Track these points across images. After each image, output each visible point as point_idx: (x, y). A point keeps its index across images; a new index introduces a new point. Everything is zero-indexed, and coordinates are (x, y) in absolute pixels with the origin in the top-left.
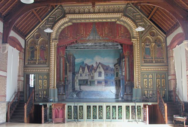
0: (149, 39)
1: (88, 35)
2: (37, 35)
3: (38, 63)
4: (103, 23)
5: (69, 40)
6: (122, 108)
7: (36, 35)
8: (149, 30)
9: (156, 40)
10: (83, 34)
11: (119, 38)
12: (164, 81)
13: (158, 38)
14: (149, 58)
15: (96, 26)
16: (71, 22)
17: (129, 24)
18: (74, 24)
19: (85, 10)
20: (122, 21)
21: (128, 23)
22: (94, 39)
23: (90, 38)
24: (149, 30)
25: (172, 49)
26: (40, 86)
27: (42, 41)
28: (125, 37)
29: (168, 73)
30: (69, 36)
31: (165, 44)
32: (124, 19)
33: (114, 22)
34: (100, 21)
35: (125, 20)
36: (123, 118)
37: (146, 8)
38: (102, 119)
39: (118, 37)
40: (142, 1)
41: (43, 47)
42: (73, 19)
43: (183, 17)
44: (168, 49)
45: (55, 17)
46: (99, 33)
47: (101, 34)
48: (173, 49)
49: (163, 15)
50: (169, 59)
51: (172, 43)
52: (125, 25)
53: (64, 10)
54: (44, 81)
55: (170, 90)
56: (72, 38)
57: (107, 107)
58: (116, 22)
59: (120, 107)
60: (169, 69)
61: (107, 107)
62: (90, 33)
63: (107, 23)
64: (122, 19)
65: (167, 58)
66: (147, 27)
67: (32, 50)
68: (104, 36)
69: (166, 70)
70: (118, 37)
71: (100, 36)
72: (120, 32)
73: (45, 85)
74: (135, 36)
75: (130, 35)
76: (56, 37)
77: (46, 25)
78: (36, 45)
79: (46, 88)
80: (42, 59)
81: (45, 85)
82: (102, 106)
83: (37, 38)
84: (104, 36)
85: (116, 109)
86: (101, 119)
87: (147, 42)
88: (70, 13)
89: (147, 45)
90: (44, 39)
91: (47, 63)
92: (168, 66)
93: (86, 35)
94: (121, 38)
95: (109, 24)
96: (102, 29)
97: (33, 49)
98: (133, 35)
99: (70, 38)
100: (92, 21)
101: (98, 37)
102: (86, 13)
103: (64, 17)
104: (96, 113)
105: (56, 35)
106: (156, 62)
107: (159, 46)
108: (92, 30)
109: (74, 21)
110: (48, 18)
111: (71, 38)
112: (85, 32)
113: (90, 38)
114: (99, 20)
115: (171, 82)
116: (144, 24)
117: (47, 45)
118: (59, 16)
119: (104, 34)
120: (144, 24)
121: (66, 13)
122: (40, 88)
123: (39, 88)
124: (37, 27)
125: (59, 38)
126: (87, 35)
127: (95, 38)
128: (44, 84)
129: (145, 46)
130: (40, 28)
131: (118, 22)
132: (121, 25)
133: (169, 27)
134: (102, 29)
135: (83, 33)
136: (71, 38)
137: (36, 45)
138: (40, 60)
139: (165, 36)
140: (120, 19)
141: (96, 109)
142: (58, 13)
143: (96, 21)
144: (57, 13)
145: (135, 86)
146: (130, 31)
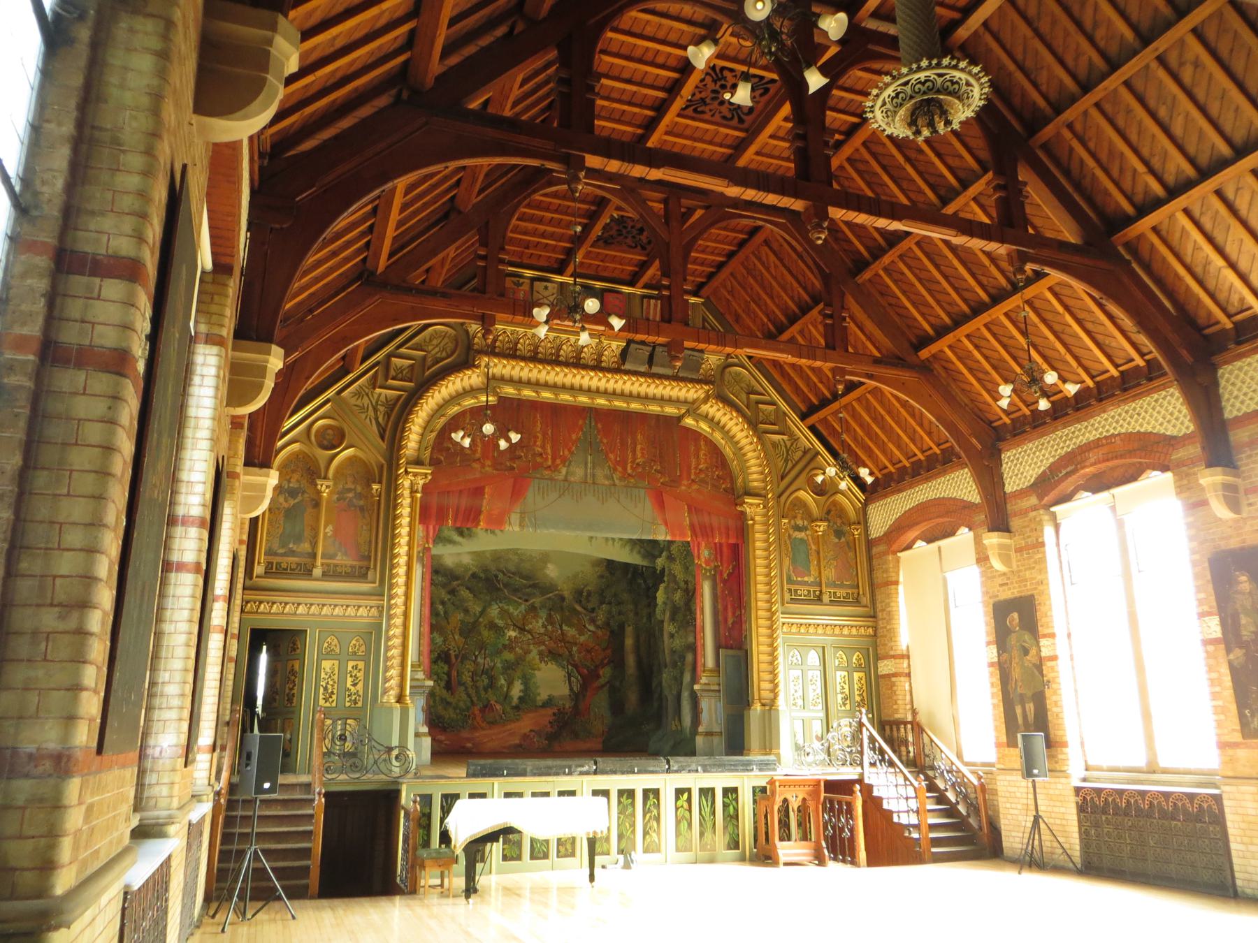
0: (802, 504)
1: (564, 460)
2: (326, 428)
3: (324, 574)
5: (478, 475)
6: (736, 800)
8: (806, 466)
9: (828, 512)
11: (689, 486)
12: (863, 681)
13: (835, 503)
14: (805, 583)
15: (600, 426)
16: (495, 394)
17: (732, 433)
18: (503, 400)
20: (706, 418)
21: (727, 428)
22: (589, 480)
24: (806, 466)
25: (895, 553)
26: (326, 689)
27: (351, 460)
28: (713, 485)
29: (875, 649)
30: (478, 455)
31: (861, 527)
32: (712, 411)
33: (671, 417)
34: (619, 404)
35: (718, 415)
37: (807, 379)
38: (659, 851)
39: (685, 482)
40: (849, 368)
41: (351, 495)
42: (502, 379)
43: (979, 447)
44: (875, 550)
45: (424, 358)
46: (612, 456)
47: (618, 463)
50: (877, 592)
51: (899, 528)
52: (717, 437)
53: (467, 332)
54: (351, 664)
55: (884, 718)
56: (494, 466)
57: (679, 792)
58: (679, 418)
59: (652, 794)
61: (679, 792)
62: (572, 453)
63: (643, 417)
64: (705, 408)
66: (799, 454)
67: (292, 502)
68: (629, 471)
69: (870, 636)
70: (685, 482)
71: (615, 470)
74: (756, 488)
75: (732, 479)
77: (378, 390)
78: (319, 482)
79: (360, 704)
80: (345, 554)
81: (354, 685)
82: (656, 792)
83: (325, 443)
84: (629, 471)
85: (713, 802)
87: (799, 516)
88: (492, 351)
89: (798, 529)
90: (360, 454)
91: (370, 574)
93: (554, 459)
94: (695, 487)
95: (653, 422)
96: (623, 444)
98: (745, 481)
99: (483, 466)
100: (583, 399)
101: (606, 471)
102: (566, 364)
103: (465, 363)
106: (326, 576)
107: (839, 534)
108: (579, 439)
109: (509, 391)
110: (389, 356)
111: (489, 462)
112: (552, 447)
114: (617, 403)
116: (789, 444)
117: (375, 487)
118: (443, 359)
119: (633, 462)
120: (789, 444)
121: (476, 347)
122: (326, 700)
123: (322, 702)
124: (330, 393)
126: (558, 461)
128: (349, 680)
130: (344, 400)
131: (689, 422)
132: (696, 435)
133: (886, 467)
134: (623, 444)
135: (543, 447)
136: (489, 462)
137: (319, 482)
139: (862, 497)
140: (698, 408)
141: (633, 804)
142: (435, 342)
143: (601, 401)
144: (431, 340)
145: (756, 697)
146: (735, 465)
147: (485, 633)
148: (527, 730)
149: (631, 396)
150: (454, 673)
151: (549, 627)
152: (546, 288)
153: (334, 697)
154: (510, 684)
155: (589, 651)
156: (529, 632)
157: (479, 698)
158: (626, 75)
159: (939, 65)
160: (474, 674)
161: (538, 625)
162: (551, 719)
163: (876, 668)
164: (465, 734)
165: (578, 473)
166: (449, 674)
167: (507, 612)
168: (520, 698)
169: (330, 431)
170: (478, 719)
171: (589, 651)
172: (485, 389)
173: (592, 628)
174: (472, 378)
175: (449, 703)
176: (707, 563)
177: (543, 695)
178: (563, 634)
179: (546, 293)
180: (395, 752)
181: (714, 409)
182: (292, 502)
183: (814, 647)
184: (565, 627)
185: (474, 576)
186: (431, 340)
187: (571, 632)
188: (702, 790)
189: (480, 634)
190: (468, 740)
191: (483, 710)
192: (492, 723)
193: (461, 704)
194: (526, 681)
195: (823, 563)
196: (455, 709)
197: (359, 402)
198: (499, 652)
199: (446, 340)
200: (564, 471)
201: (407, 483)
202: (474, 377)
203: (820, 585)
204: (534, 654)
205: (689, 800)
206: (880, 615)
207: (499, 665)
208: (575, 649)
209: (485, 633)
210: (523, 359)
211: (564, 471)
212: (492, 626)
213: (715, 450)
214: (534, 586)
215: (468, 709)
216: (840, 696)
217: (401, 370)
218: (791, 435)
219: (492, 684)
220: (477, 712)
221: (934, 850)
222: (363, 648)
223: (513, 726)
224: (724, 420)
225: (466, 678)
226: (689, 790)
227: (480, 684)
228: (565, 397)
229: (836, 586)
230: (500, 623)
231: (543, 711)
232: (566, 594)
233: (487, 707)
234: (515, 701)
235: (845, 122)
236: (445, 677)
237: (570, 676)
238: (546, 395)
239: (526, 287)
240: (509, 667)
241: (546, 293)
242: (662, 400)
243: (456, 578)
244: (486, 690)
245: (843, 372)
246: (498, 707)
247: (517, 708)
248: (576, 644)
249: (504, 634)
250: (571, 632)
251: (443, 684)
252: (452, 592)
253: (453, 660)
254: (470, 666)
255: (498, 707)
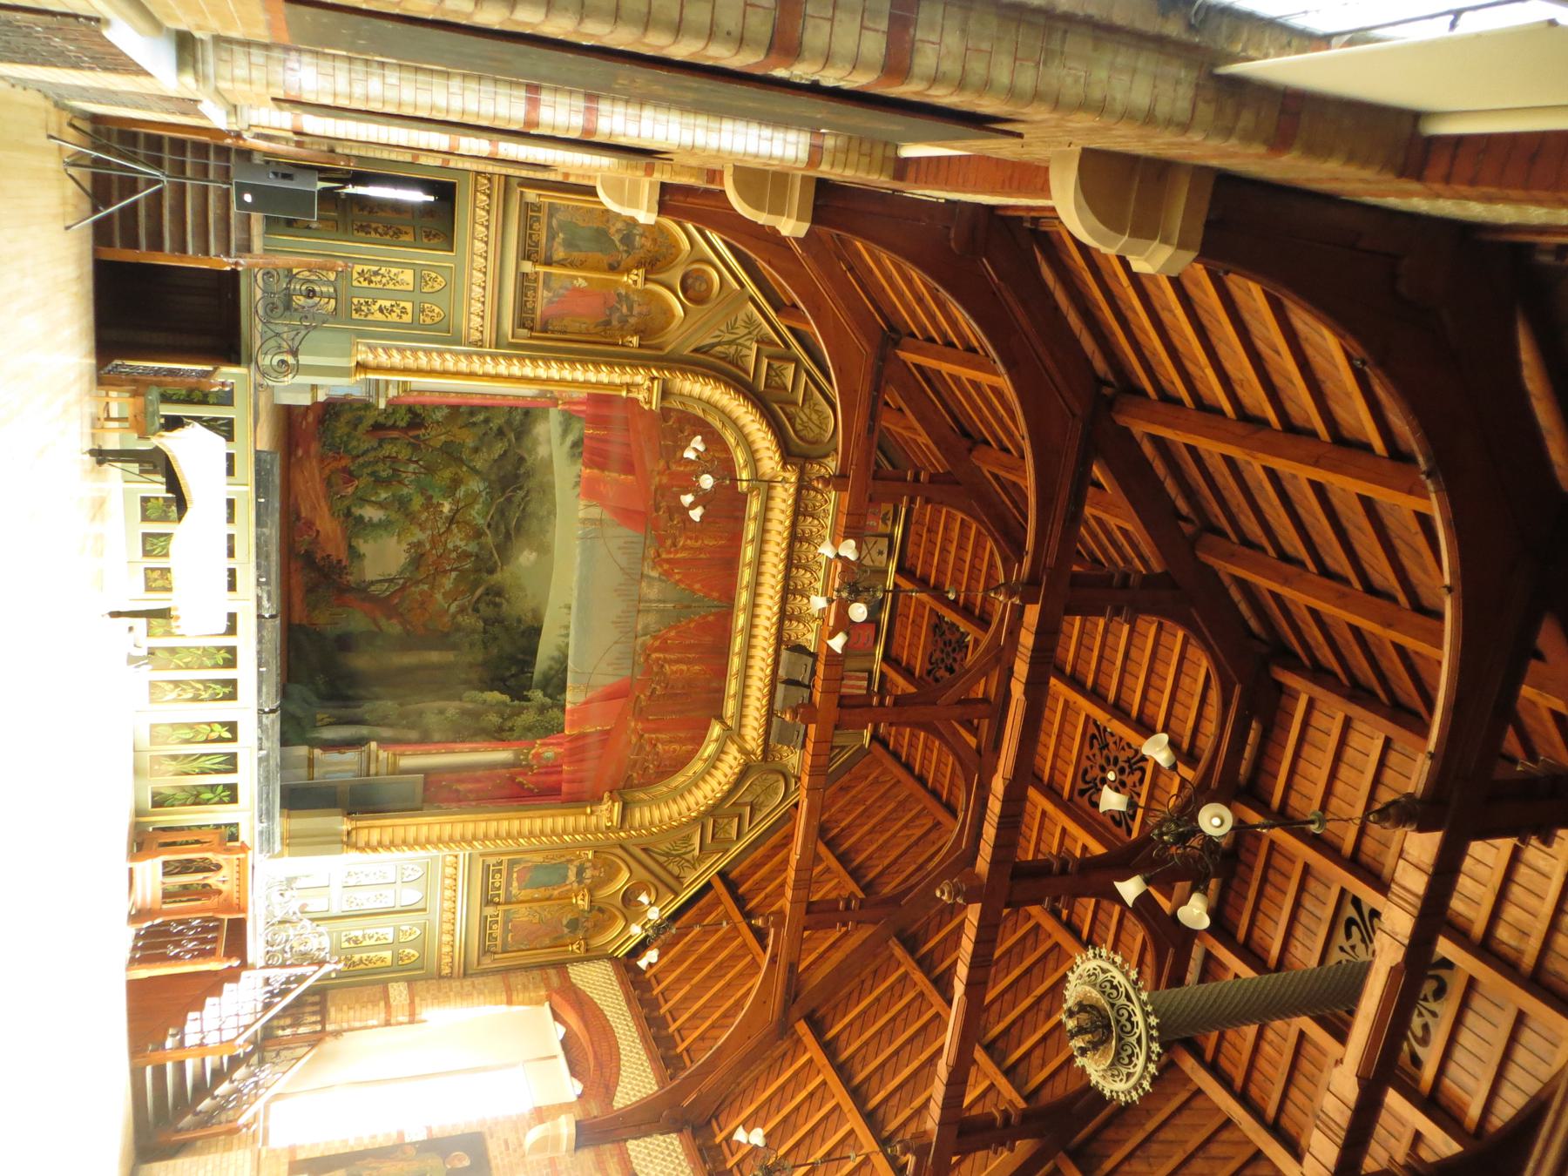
1: (668, 574)
3: (525, 275)
4: (721, 651)
6: (221, 802)
7: (704, 271)
9: (601, 910)
10: (674, 545)
12: (379, 964)
13: (613, 919)
14: (509, 884)
15: (711, 618)
16: (751, 490)
18: (742, 499)
19: (806, 568)
20: (721, 751)
23: (650, 586)
25: (549, 998)
26: (376, 273)
27: (668, 312)
28: (635, 762)
29: (426, 978)
30: (674, 467)
31: (581, 953)
34: (738, 643)
36: (156, 706)
39: (640, 726)
40: (784, 932)
41: (625, 310)
42: (769, 498)
43: (686, 1103)
44: (552, 972)
45: (795, 403)
46: (673, 633)
47: (665, 641)
48: (547, 1004)
49: (721, 968)
50: (498, 978)
52: (697, 766)
53: (826, 456)
54: (409, 306)
55: (331, 993)
56: (660, 487)
57: (232, 727)
58: (720, 718)
60: (445, 984)
61: (232, 727)
63: (722, 673)
64: (733, 750)
65: (506, 971)
66: (676, 871)
67: (616, 238)
68: (654, 656)
70: (640, 726)
71: (655, 638)
72: (662, 736)
73: (381, 310)
74: (632, 816)
75: (643, 786)
76: (681, 395)
77: (755, 346)
78: (641, 272)
79: (355, 316)
80: (550, 302)
82: (232, 696)
83: (690, 281)
84: (654, 656)
85: (217, 772)
86: (151, 694)
88: (802, 487)
89: (580, 871)
90: (676, 323)
92: (465, 975)
94: (634, 740)
96: (690, 648)
97: (621, 248)
99: (660, 473)
100: (743, 597)
101: (653, 627)
102: (787, 577)
103: (788, 453)
104: (188, 667)
105: (690, 396)
106: (523, 278)
107: (574, 925)
108: (694, 592)
109: (754, 506)
110: (797, 361)
113: (650, 586)
115: (375, 1003)
117: (635, 340)
118: (793, 427)
119: (665, 660)
121: (808, 466)
122: (361, 274)
123: (358, 268)
124: (751, 288)
125: (670, 410)
126: (666, 566)
127: (648, 611)
128: (387, 304)
129: (577, 863)
130: (743, 305)
131: (716, 730)
132: (699, 739)
134: (690, 648)
135: (684, 548)
136: (665, 480)
137: (641, 272)
138: (546, 285)
139: (621, 953)
141: (216, 666)
142: (814, 417)
143: (741, 620)
144: (817, 412)
145: (360, 824)
146: (662, 789)
147: (447, 474)
148: (319, 525)
149: (747, 657)
150: (395, 434)
151: (454, 555)
152: (881, 553)
153: (365, 284)
154: (381, 505)
155: (423, 603)
156: (448, 529)
157: (363, 466)
158: (1134, 653)
159: (1151, 1038)
160: (394, 459)
161: (457, 540)
162: (334, 559)
163: (396, 980)
164: (315, 447)
165: (652, 592)
166: (394, 427)
167: (475, 501)
168: (361, 517)
169: (704, 287)
170: (335, 464)
171: (423, 603)
172: (756, 477)
173: (453, 608)
174: (770, 460)
175: (355, 427)
176: (537, 756)
177: (365, 547)
178: (445, 572)
179: (874, 552)
180: (290, 360)
181: (732, 761)
182: (616, 238)
183: (425, 897)
184: (454, 574)
185: (522, 460)
186: (817, 412)
187: (448, 582)
188: (234, 756)
189: (447, 466)
190: (307, 452)
191: (345, 470)
192: (328, 483)
193: (354, 443)
194: (385, 525)
195: (535, 906)
196: (349, 435)
197: (739, 323)
198: (422, 491)
199: (817, 430)
200: (654, 574)
201: (639, 379)
202: (772, 464)
203: (507, 903)
204: (419, 535)
205: (220, 740)
206: (468, 982)
207: (405, 491)
208: (426, 587)
209: (447, 474)
210: (794, 524)
211: (654, 574)
212: (456, 482)
213: (680, 763)
214: (508, 536)
215: (347, 451)
216: (359, 934)
217: (780, 374)
218: (700, 860)
219: (379, 482)
220: (343, 463)
221: (149, 1070)
222: (428, 321)
223: (325, 509)
224: (718, 774)
225: (389, 449)
226: (234, 739)
227: (380, 466)
228: (746, 575)
229: (505, 923)
230: (460, 493)
231: (343, 546)
232: (498, 576)
233: (350, 476)
234: (357, 511)
235: (1083, 921)
236: (390, 423)
237: (391, 581)
238: (749, 553)
239: (882, 528)
240: (402, 504)
241: (874, 552)
242: (743, 696)
243: (519, 437)
244: (373, 474)
245: (779, 925)
246: (350, 490)
247: (348, 514)
248: (432, 588)
249: (445, 498)
250: (448, 582)
251: (381, 419)
252: (501, 433)
253: (411, 433)
254: (405, 454)
255: (350, 490)
